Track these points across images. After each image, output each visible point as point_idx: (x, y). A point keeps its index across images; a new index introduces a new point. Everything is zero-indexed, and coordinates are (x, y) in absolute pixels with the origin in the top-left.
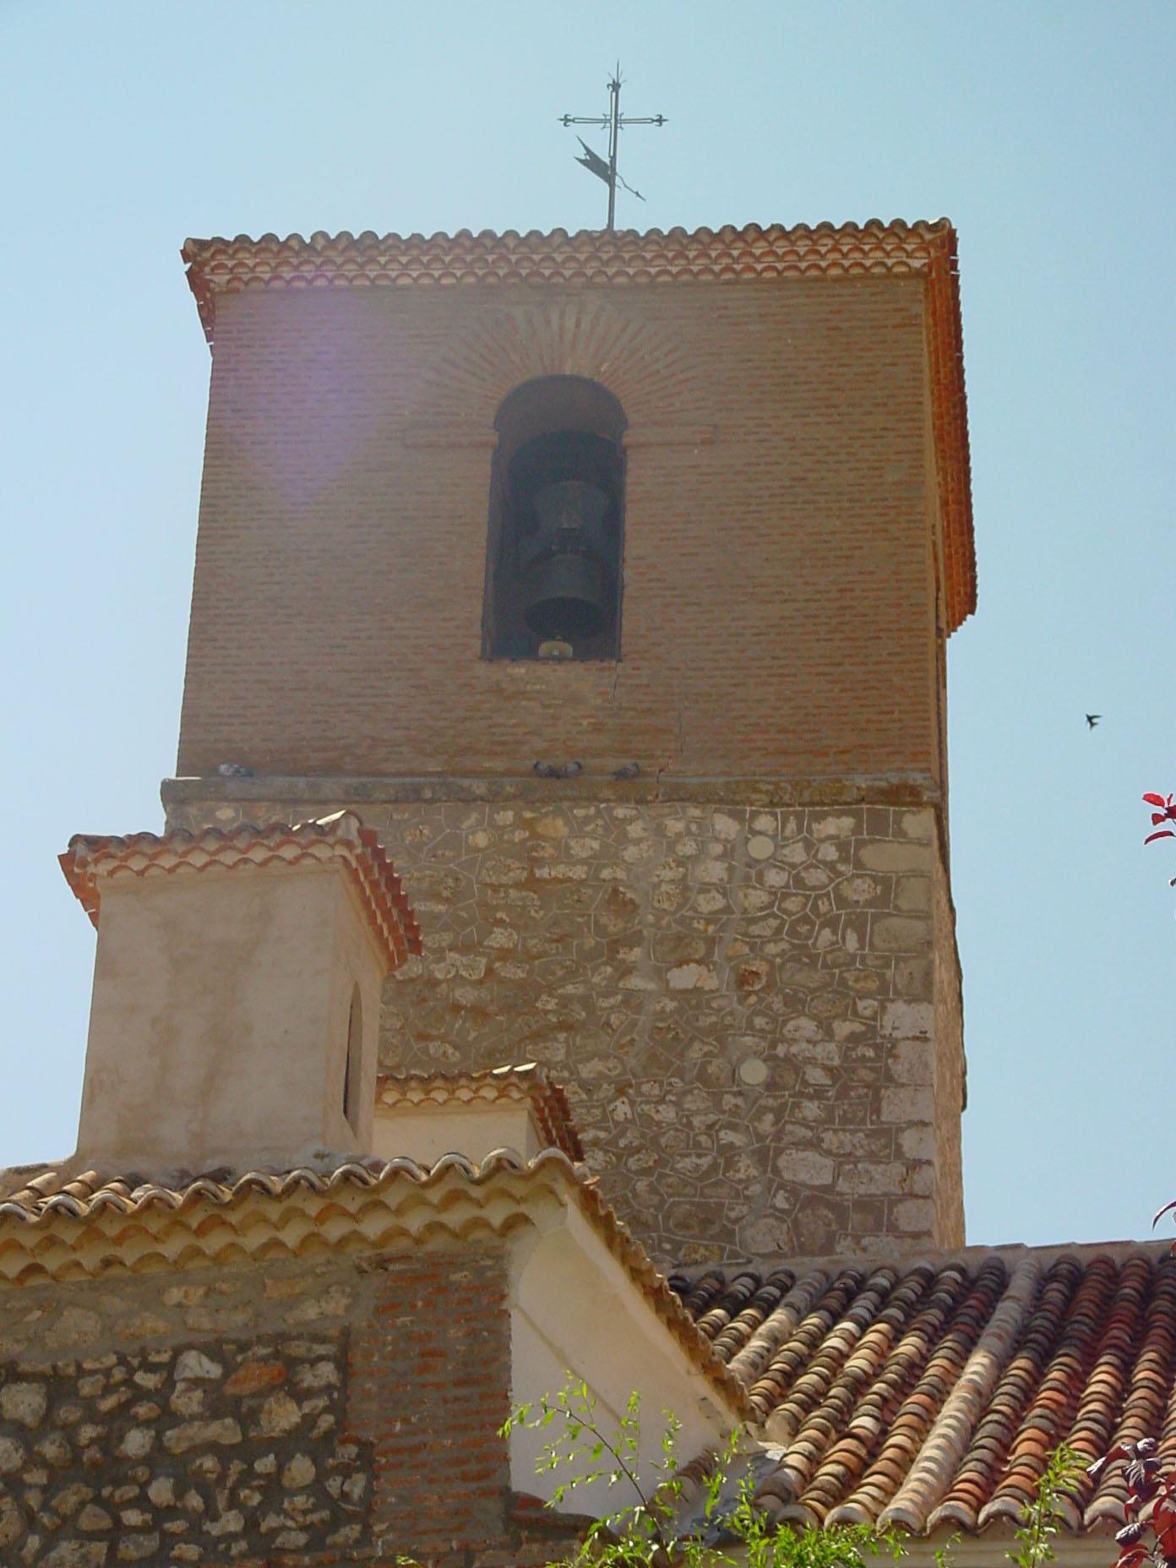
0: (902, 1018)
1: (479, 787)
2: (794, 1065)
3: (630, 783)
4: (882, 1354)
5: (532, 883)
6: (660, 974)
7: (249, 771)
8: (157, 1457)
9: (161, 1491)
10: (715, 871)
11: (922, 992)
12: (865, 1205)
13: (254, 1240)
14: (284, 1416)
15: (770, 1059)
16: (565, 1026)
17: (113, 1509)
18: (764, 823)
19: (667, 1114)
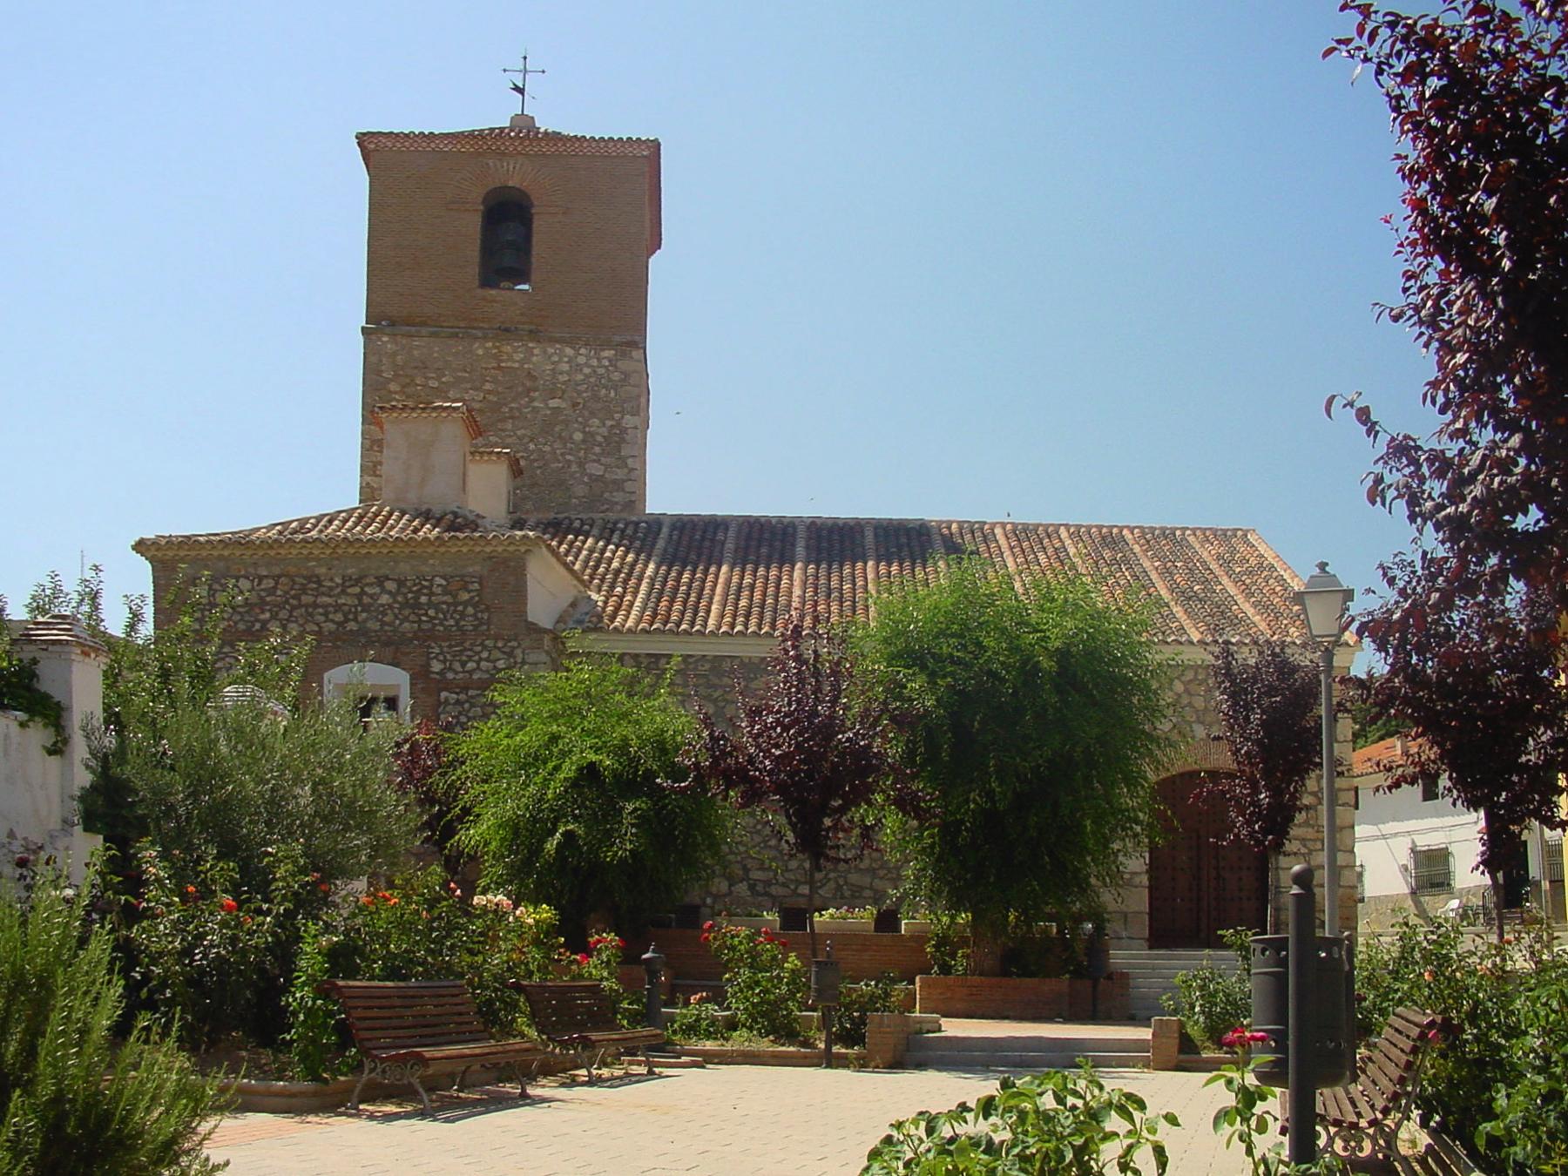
0: (629, 421)
1: (480, 334)
2: (592, 435)
3: (534, 335)
4: (623, 558)
5: (499, 368)
6: (545, 401)
7: (393, 324)
8: (430, 604)
9: (431, 612)
10: (566, 367)
11: (635, 413)
12: (614, 482)
13: (454, 550)
14: (465, 596)
15: (584, 432)
16: (512, 418)
17: (419, 616)
18: (583, 351)
19: (547, 448)
